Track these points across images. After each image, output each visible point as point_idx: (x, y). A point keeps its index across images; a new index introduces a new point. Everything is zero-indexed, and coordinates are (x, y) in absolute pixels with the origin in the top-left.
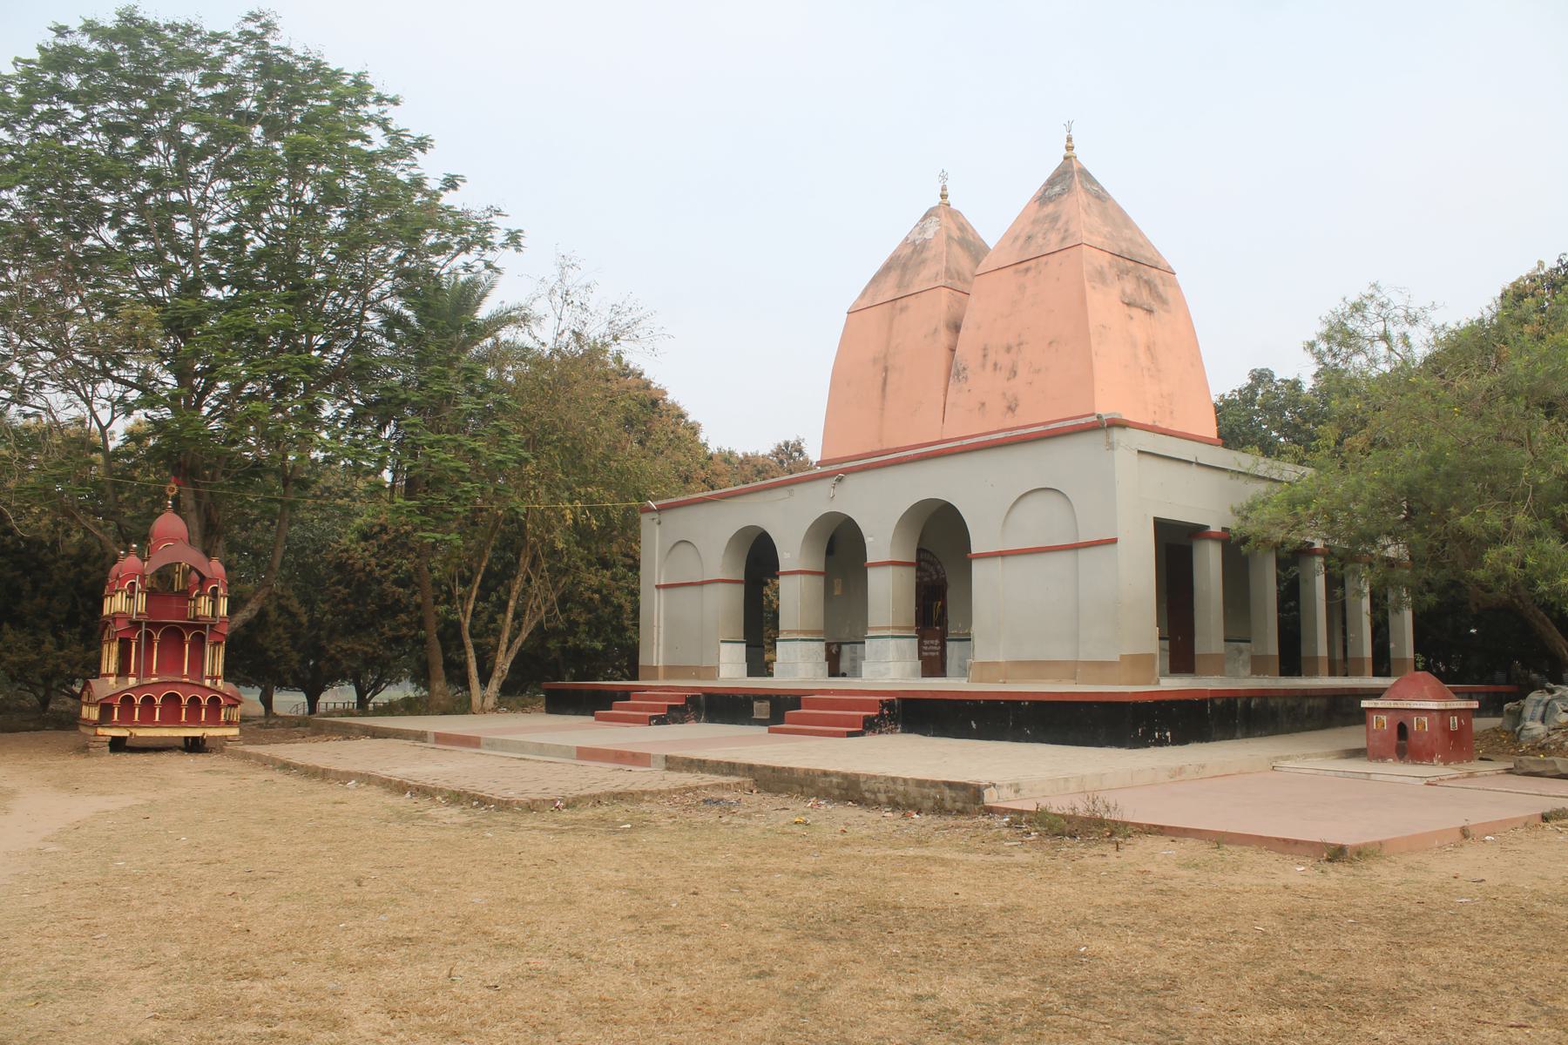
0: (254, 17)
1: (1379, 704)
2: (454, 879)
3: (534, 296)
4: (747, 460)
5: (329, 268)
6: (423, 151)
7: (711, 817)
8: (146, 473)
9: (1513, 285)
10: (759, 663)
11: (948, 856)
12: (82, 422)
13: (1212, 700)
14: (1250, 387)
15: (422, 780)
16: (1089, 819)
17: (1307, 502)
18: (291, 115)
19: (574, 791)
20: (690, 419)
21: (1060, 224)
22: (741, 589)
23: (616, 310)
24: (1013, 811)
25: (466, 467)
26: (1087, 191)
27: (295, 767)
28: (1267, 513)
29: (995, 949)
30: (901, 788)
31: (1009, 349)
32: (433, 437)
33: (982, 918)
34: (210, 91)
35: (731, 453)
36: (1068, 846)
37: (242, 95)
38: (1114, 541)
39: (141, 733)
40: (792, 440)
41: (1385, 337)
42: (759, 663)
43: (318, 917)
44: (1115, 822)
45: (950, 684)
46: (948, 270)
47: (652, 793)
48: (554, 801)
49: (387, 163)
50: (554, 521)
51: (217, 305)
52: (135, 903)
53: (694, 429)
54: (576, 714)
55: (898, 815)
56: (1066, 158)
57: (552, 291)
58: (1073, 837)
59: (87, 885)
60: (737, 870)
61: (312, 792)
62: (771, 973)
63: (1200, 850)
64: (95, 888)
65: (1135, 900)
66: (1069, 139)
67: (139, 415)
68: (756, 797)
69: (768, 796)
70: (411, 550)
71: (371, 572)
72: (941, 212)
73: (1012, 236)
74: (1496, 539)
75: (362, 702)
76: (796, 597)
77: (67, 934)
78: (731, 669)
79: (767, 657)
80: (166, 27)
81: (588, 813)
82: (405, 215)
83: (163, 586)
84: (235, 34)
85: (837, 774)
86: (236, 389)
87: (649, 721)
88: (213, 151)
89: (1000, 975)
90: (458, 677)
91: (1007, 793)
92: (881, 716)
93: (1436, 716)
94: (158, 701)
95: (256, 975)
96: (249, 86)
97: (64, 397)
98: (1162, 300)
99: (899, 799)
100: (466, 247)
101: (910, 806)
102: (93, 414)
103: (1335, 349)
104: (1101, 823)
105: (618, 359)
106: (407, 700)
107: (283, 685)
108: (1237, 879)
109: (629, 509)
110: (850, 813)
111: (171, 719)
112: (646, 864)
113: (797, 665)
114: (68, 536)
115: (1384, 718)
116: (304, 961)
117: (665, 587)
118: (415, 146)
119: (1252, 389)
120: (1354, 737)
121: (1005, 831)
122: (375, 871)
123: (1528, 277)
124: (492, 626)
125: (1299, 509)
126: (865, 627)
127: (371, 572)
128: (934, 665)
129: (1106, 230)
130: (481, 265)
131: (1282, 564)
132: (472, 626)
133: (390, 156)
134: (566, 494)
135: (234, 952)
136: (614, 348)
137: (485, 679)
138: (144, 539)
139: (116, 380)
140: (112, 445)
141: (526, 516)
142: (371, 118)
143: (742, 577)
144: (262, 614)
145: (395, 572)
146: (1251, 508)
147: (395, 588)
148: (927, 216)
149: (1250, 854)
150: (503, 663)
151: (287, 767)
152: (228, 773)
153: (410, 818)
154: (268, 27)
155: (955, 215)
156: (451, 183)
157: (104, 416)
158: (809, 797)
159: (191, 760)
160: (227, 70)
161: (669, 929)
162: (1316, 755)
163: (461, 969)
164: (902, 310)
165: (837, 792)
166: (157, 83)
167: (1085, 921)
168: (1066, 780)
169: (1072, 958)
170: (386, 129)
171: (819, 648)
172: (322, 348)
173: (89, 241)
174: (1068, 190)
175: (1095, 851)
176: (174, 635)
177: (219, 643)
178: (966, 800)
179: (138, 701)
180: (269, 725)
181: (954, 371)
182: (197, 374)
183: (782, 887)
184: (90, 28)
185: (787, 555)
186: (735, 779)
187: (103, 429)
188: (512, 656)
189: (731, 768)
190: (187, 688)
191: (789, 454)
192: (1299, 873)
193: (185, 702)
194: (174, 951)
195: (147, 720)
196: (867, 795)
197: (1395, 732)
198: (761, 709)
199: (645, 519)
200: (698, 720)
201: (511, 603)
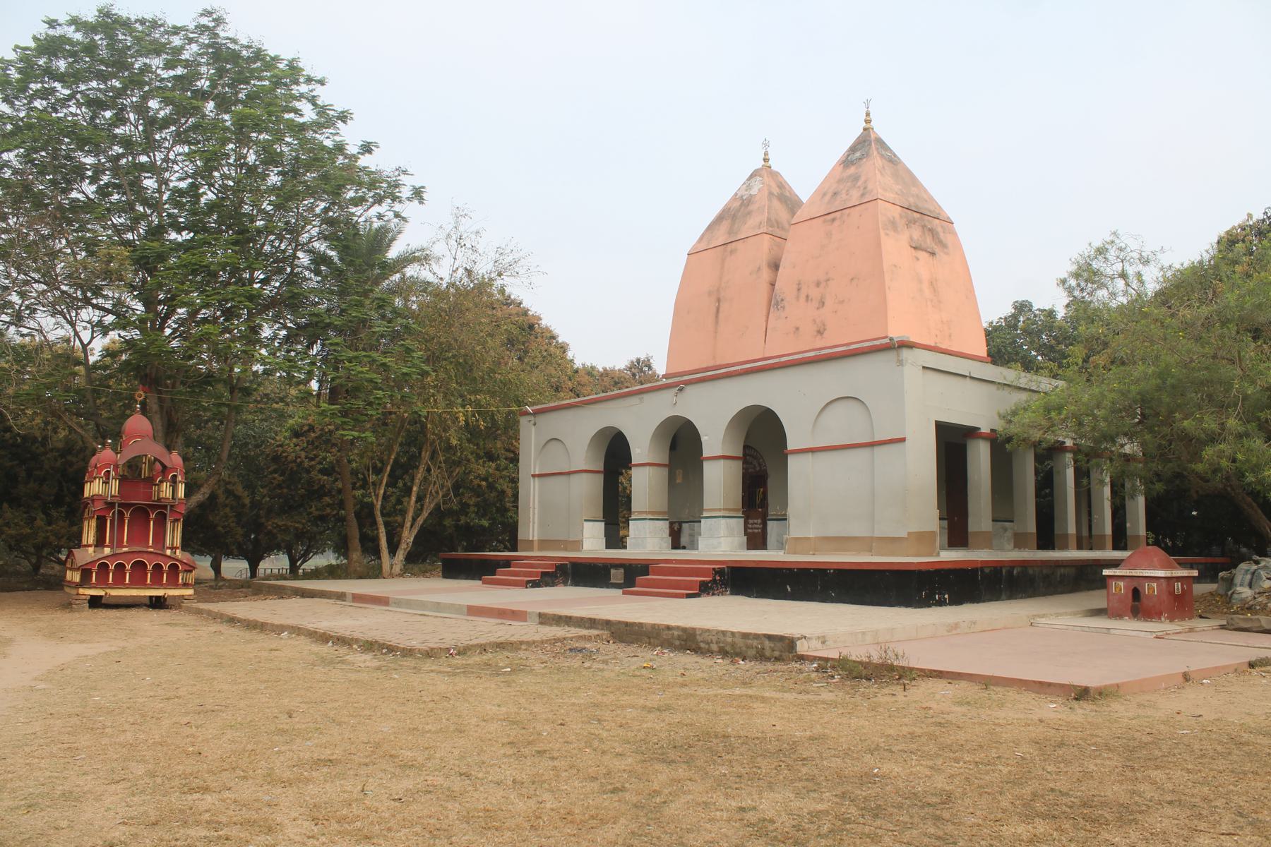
0: (207, 13)
1: (1118, 572)
3: (434, 240)
4: (606, 373)
5: (268, 217)
6: (345, 122)
7: (576, 662)
8: (120, 382)
9: (1227, 233)
10: (615, 538)
11: (767, 694)
12: (68, 341)
13: (982, 569)
14: (1013, 316)
17: (1059, 409)
19: (465, 641)
20: (560, 340)
21: (859, 183)
22: (600, 478)
23: (500, 251)
24: (821, 658)
26: (882, 156)
27: (239, 620)
28: (1027, 418)
29: (804, 770)
30: (729, 640)
31: (818, 284)
32: (352, 354)
33: (794, 746)
35: (593, 368)
36: (865, 687)
37: (199, 76)
38: (903, 440)
39: (114, 592)
40: (643, 357)
41: (1123, 275)
42: (615, 538)
44: (903, 668)
46: (769, 220)
47: (528, 643)
48: (448, 649)
51: (179, 246)
53: (563, 348)
54: (467, 579)
55: (727, 661)
59: (70, 716)
60: (596, 705)
61: (252, 641)
62: (623, 789)
64: (76, 718)
65: (918, 731)
66: (868, 114)
67: (113, 335)
68: (612, 646)
69: (622, 646)
70: (334, 445)
71: (302, 462)
73: (821, 193)
74: (1213, 439)
75: (294, 568)
76: (645, 484)
77: (53, 756)
79: (622, 533)
81: (476, 659)
82: (329, 174)
83: (132, 474)
85: (678, 628)
86: (193, 314)
87: (526, 585)
88: (174, 122)
90: (372, 549)
91: (815, 644)
92: (714, 581)
93: (1164, 583)
94: (128, 567)
95: (206, 790)
96: (203, 69)
97: (53, 320)
99: (728, 648)
100: (379, 200)
101: (737, 655)
102: (77, 334)
103: (1083, 284)
104: (891, 668)
107: (230, 555)
108: (1001, 714)
110: (688, 659)
111: (139, 581)
112: (522, 701)
113: (647, 539)
114: (56, 433)
115: (1122, 584)
116: (245, 778)
117: (540, 476)
118: (339, 118)
119: (1014, 317)
120: (1097, 599)
121: (814, 675)
124: (399, 507)
125: (1053, 414)
126: (701, 509)
127: (302, 462)
128: (757, 540)
130: (391, 214)
131: (1039, 459)
132: (383, 507)
133: (317, 126)
134: (460, 401)
135: (188, 771)
136: (498, 283)
138: (117, 435)
139: (95, 307)
140: (92, 359)
141: (426, 418)
142: (302, 96)
143: (601, 467)
144: (213, 497)
146: (1014, 413)
147: (320, 476)
148: (752, 176)
149: (1012, 694)
150: (408, 537)
151: (232, 620)
152: (185, 625)
153: (331, 662)
155: (775, 175)
156: (367, 148)
157: (86, 336)
159: (155, 615)
160: (186, 56)
162: (1066, 614)
163: (372, 785)
164: (732, 252)
165: (677, 643)
166: (130, 67)
167: (877, 748)
169: (867, 778)
170: (315, 104)
171: (664, 526)
172: (262, 281)
173: (74, 195)
174: (866, 155)
175: (886, 691)
176: (141, 513)
177: (178, 520)
178: (781, 650)
179: (112, 567)
180: (219, 587)
181: (773, 302)
182: (160, 302)
183: (633, 719)
184: (74, 22)
185: (638, 451)
186: (595, 632)
187: (84, 346)
188: (415, 531)
189: (592, 623)
191: (640, 368)
192: (1051, 709)
193: (150, 568)
194: (140, 770)
195: (119, 582)
196: (702, 645)
198: (617, 575)
199: (523, 421)
200: (565, 584)
201: (415, 489)
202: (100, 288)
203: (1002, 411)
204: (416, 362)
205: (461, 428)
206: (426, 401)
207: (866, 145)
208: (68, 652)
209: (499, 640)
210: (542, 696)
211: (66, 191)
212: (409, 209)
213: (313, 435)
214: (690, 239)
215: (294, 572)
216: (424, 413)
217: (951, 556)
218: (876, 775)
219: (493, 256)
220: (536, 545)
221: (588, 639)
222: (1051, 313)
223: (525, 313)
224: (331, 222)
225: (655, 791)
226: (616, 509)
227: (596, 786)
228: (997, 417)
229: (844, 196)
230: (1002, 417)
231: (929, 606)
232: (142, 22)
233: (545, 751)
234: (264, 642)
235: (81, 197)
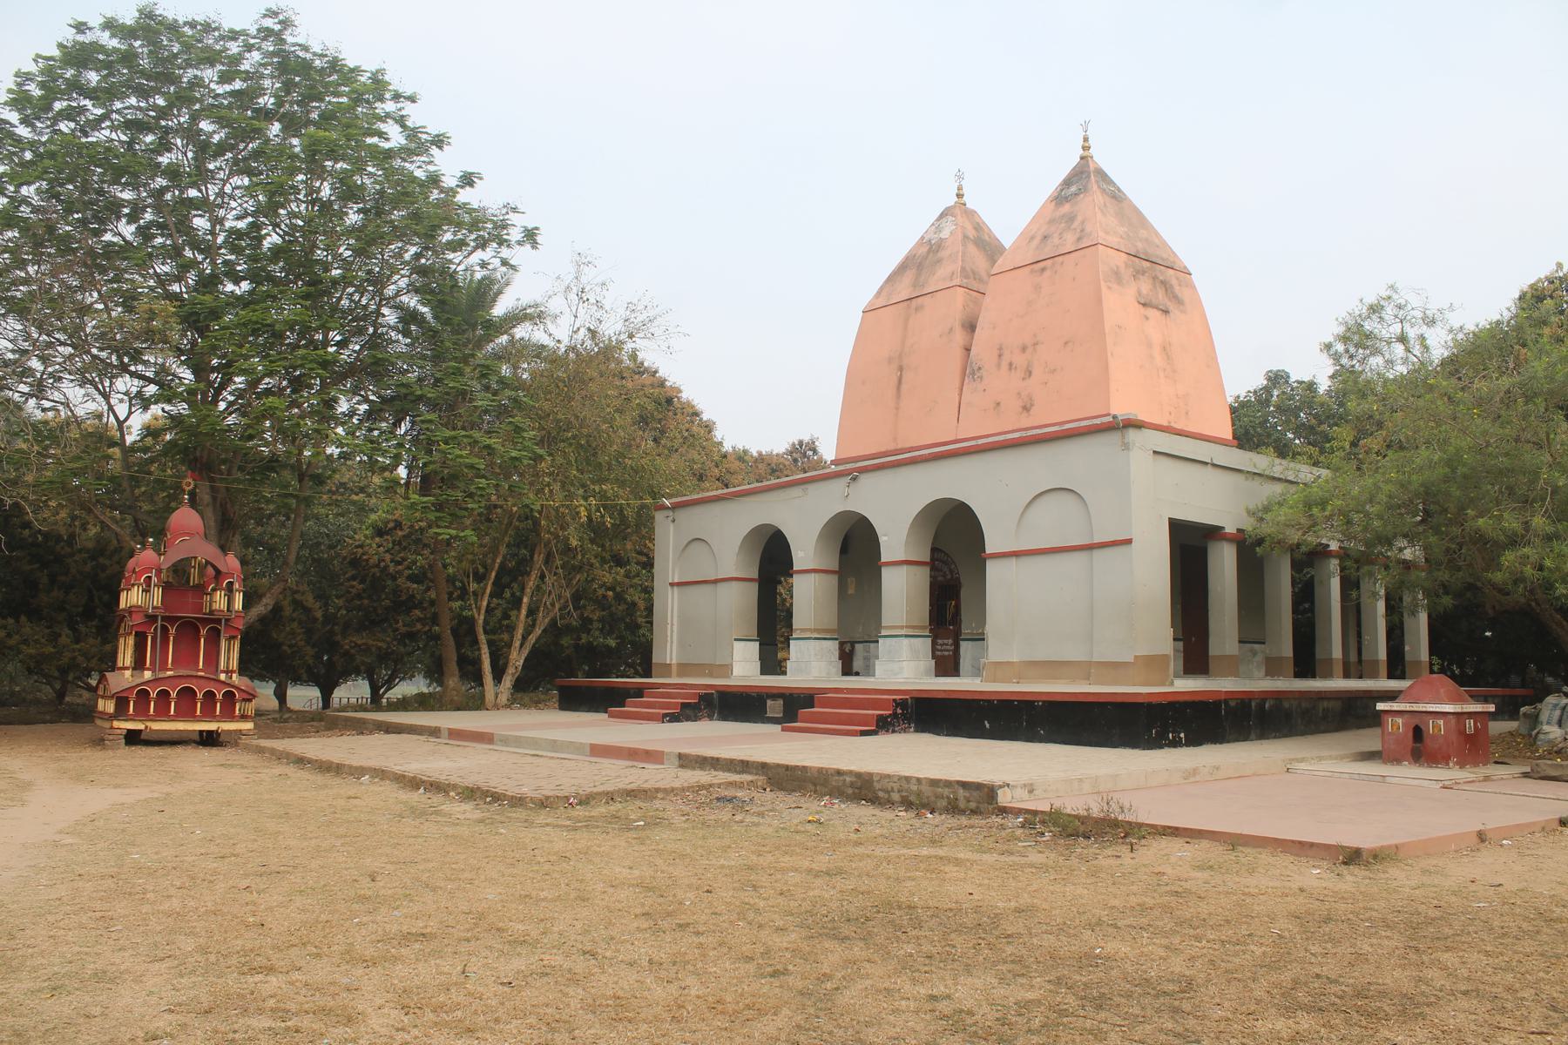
0: (271, 13)
1: (1395, 706)
2: (467, 875)
3: (549, 294)
4: (761, 458)
5: (346, 265)
6: (440, 148)
7: (725, 814)
9: (1531, 286)
10: (772, 662)
11: (961, 856)
12: (99, 416)
16: (1103, 820)
17: (1323, 504)
18: (308, 112)
20: (705, 417)
22: (755, 586)
23: (631, 307)
24: (1028, 811)
27: (310, 761)
28: (1283, 514)
29: (1009, 949)
30: (915, 788)
31: (1024, 349)
32: (448, 433)
33: (996, 919)
34: (228, 88)
35: (745, 452)
36: (1082, 847)
37: (261, 91)
38: (1129, 542)
39: (156, 726)
40: (806, 439)
41: (1402, 339)
42: (772, 662)
44: (1130, 823)
45: (963, 684)
46: (963, 269)
48: (567, 798)
49: (404, 160)
52: (150, 896)
53: (709, 427)
55: (912, 814)
57: (568, 288)
59: (103, 878)
60: (750, 868)
62: (785, 972)
63: (1215, 852)
64: (110, 881)
65: (1150, 902)
66: (1086, 139)
67: (156, 410)
68: (769, 795)
69: (781, 794)
70: (426, 546)
71: (386, 567)
72: (958, 211)
73: (1027, 236)
74: (1514, 541)
76: (809, 595)
77: (82, 926)
79: (780, 655)
80: (185, 23)
81: (601, 809)
82: (420, 212)
83: (179, 580)
84: (253, 31)
85: (851, 772)
86: (253, 384)
88: (232, 148)
89: (1015, 976)
90: (471, 671)
91: (1021, 793)
92: (895, 715)
93: (1453, 720)
94: (174, 695)
95: (271, 970)
96: (267, 83)
97: (83, 391)
99: (912, 798)
100: (482, 244)
101: (924, 806)
102: (111, 408)
103: (1352, 350)
104: (1115, 824)
106: (421, 695)
107: (297, 680)
109: (643, 507)
110: (864, 812)
111: (186, 713)
112: (659, 862)
113: (811, 664)
115: (1400, 721)
117: (679, 584)
119: (1267, 389)
120: (1369, 739)
121: (1019, 832)
123: (1547, 278)
125: (1315, 510)
126: (879, 626)
128: (947, 665)
130: (497, 262)
131: (1297, 566)
132: (486, 622)
134: (581, 491)
135: (249, 946)
136: (629, 346)
138: (160, 533)
139: (134, 375)
140: (129, 439)
141: (540, 513)
142: (388, 115)
143: (756, 576)
144: (277, 609)
146: (1267, 509)
148: (942, 215)
149: (1265, 857)
150: (517, 659)
151: (301, 761)
152: (243, 767)
153: (423, 813)
154: (286, 24)
155: (970, 214)
156: (468, 180)
161: (682, 926)
162: (1331, 758)
165: (850, 791)
166: (175, 80)
167: (1100, 923)
169: (1088, 960)
170: (403, 126)
172: (338, 344)
173: (108, 237)
174: (1084, 190)
175: (1109, 852)
176: (189, 629)
177: (234, 637)
178: (979, 800)
179: (153, 695)
180: (284, 720)
181: (969, 371)
182: (213, 369)
183: (796, 885)
184: (110, 25)
185: (801, 554)
186: (748, 777)
187: (120, 423)
188: (526, 652)
189: (744, 766)
190: (202, 682)
191: (803, 453)
192: (1315, 875)
193: (200, 696)
194: (188, 944)
195: (162, 713)
196: (881, 794)
197: (1411, 734)
198: (774, 707)
199: (659, 516)
200: (711, 718)
201: (525, 600)
203: (1252, 506)
206: (540, 491)
207: (1084, 177)
210: (683, 856)
211: (98, 233)
212: (520, 255)
214: (867, 295)
215: (376, 701)
217: (1187, 685)
218: (1098, 956)
219: (622, 312)
220: (674, 669)
221: (739, 786)
222: (1311, 386)
224: (423, 271)
226: (773, 628)
227: (751, 967)
229: (1056, 241)
230: (1251, 513)
231: (1161, 747)
232: (192, 25)
233: (688, 925)
234: (340, 788)
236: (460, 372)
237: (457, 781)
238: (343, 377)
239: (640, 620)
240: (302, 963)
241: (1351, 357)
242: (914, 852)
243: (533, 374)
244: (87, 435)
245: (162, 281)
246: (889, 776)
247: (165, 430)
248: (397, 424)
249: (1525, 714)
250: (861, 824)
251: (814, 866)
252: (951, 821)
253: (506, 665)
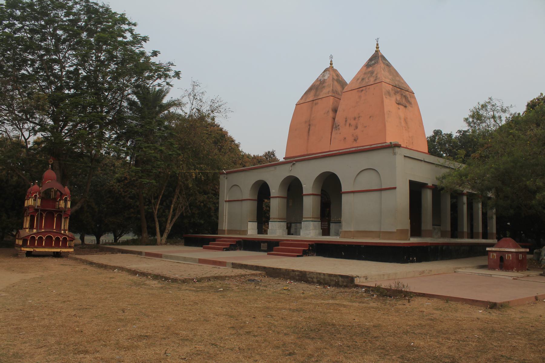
1: (493, 249)
2: (160, 310)
3: (181, 95)
4: (255, 157)
5: (109, 83)
6: (146, 42)
7: (252, 286)
8: (41, 157)
9: (531, 101)
10: (262, 229)
11: (345, 303)
12: (18, 137)
14: (433, 136)
15: (143, 270)
16: (396, 290)
17: (466, 175)
18: (97, 29)
19: (200, 276)
21: (374, 75)
22: (256, 203)
23: (213, 101)
24: (366, 286)
25: (158, 156)
26: (384, 63)
27: (95, 263)
29: (378, 343)
30: (322, 277)
32: (146, 145)
34: (68, 18)
35: (249, 155)
36: (389, 300)
37: (79, 20)
38: (395, 188)
39: (37, 250)
40: (271, 151)
41: (494, 117)
43: (109, 326)
44: (407, 292)
46: (333, 90)
49: (132, 46)
50: (189, 177)
51: (68, 96)
52: (36, 318)
53: (237, 146)
54: (195, 246)
56: (376, 51)
57: (190, 94)
58: (390, 297)
59: (17, 310)
60: (268, 308)
61: (101, 273)
62: (294, 353)
63: (441, 303)
64: (20, 312)
66: (377, 45)
67: (39, 135)
68: (267, 279)
69: (271, 279)
72: (330, 70)
73: (356, 79)
75: (116, 240)
76: (276, 206)
77: (8, 332)
78: (251, 231)
82: (138, 66)
83: (46, 197)
85: (298, 271)
86: (75, 126)
87: (223, 250)
88: (68, 41)
89: (385, 355)
91: (363, 280)
92: (309, 250)
94: (44, 238)
95: (86, 352)
96: (82, 17)
97: (12, 127)
98: (410, 103)
99: (322, 281)
100: (160, 77)
101: (326, 284)
102: (22, 134)
103: (475, 121)
104: (401, 292)
105: (213, 119)
106: (133, 240)
107: (89, 234)
109: (215, 173)
110: (303, 286)
111: (49, 245)
112: (232, 305)
113: (276, 230)
114: (12, 178)
115: (495, 254)
116: (105, 345)
117: (229, 201)
118: (143, 40)
120: (483, 261)
121: (364, 294)
122: (129, 306)
123: (537, 98)
124: (164, 214)
125: (463, 178)
128: (326, 232)
129: (390, 77)
130: (165, 84)
131: (452, 197)
132: (157, 214)
133: (132, 43)
134: (193, 167)
135: (77, 341)
136: (212, 115)
137: (162, 236)
138: (40, 179)
139: (31, 122)
140: (29, 146)
141: (179, 174)
142: (126, 30)
144: (82, 208)
145: (129, 194)
148: (325, 71)
149: (459, 305)
150: (169, 227)
151: (91, 263)
152: (70, 265)
153: (139, 285)
155: (335, 71)
156: (155, 54)
157: (26, 134)
158: (287, 279)
159: (56, 260)
160: (74, 10)
161: (248, 333)
162: (469, 267)
164: (316, 104)
165: (297, 278)
166: (48, 15)
168: (384, 275)
169: (409, 348)
170: (132, 33)
171: (284, 224)
172: (106, 112)
173: (23, 72)
174: (377, 63)
175: (400, 302)
176: (50, 215)
177: (67, 218)
178: (348, 282)
179: (37, 238)
180: (83, 248)
181: (334, 126)
182: (61, 121)
183: (287, 315)
185: (273, 191)
186: (259, 272)
187: (26, 140)
188: (172, 225)
189: (257, 268)
191: (270, 156)
192: (480, 313)
194: (52, 340)
195: (40, 245)
196: (309, 279)
197: (499, 259)
198: (264, 246)
199: (222, 177)
200: (240, 250)
201: (172, 206)
202: (34, 113)
204: (175, 149)
205: (193, 179)
206: (178, 167)
207: (377, 58)
208: (15, 277)
209: (216, 275)
210: (241, 303)
211: (20, 70)
212: (174, 81)
213: (126, 182)
215: (116, 242)
216: (178, 172)
217: (414, 240)
218: (413, 346)
219: (209, 103)
220: (226, 232)
222: (450, 135)
223: (221, 129)
224: (137, 86)
225: (310, 355)
226: (263, 218)
227: (279, 351)
228: (435, 179)
229: (367, 80)
230: (438, 179)
233: (250, 332)
235: (25, 72)
236: (151, 123)
237: (151, 272)
238: (107, 124)
239: (212, 214)
240: (99, 349)
241: (475, 123)
242: (326, 302)
243: (176, 125)
244: (13, 143)
245: (42, 89)
246: (312, 272)
247: (42, 142)
248: (127, 141)
249: (536, 252)
250: (303, 290)
251: (291, 307)
252: (338, 290)
253: (165, 229)
